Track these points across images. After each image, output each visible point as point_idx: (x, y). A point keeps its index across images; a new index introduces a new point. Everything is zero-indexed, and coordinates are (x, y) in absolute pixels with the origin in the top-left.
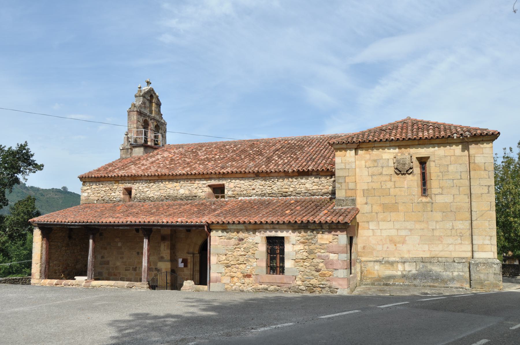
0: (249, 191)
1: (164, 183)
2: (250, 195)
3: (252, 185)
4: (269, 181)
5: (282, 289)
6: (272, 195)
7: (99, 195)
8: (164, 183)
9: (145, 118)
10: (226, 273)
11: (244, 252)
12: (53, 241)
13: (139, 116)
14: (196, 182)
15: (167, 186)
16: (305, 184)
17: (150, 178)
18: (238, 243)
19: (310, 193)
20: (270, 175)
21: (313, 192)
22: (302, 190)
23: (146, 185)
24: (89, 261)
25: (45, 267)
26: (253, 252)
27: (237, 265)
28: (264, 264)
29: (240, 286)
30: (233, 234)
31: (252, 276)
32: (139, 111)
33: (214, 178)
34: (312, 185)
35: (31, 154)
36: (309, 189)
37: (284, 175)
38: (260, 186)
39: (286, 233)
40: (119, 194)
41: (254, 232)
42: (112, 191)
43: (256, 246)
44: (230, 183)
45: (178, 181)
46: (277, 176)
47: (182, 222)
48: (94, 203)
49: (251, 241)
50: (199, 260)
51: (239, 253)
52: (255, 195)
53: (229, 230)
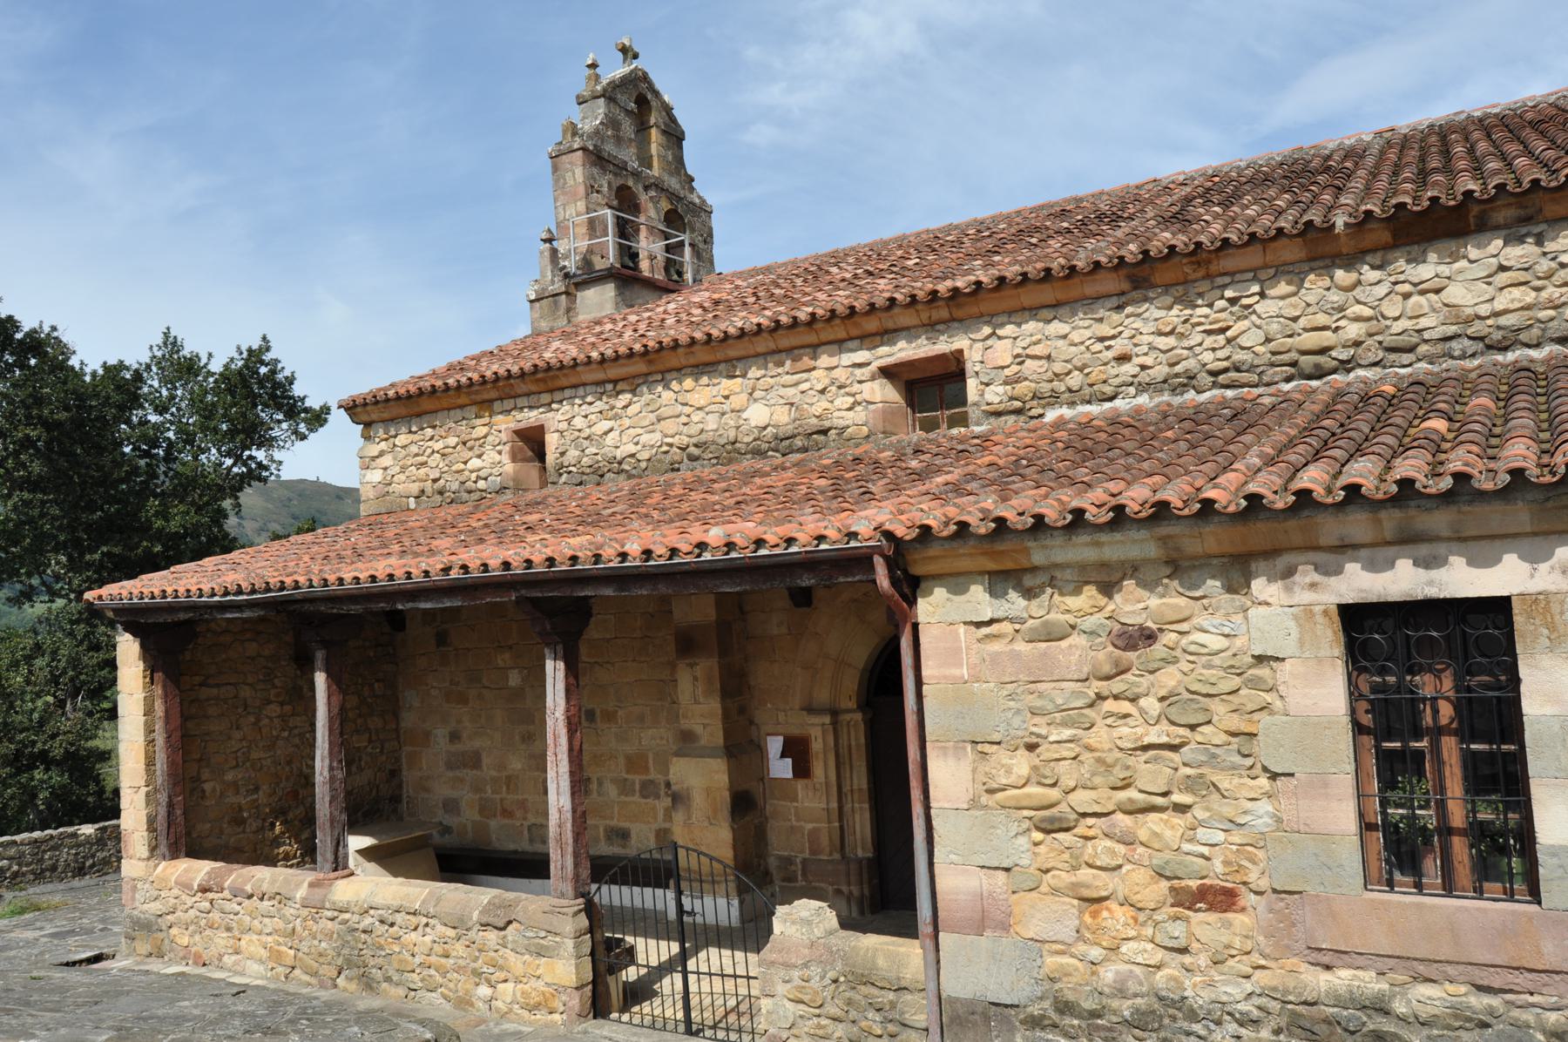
0: (1096, 373)
1: (675, 385)
2: (1108, 390)
3: (1113, 337)
4: (1210, 305)
5: (1528, 1016)
6: (1233, 375)
7: (423, 471)
8: (675, 385)
9: (620, 182)
10: (1047, 871)
11: (1164, 726)
12: (210, 681)
13: (595, 171)
14: (819, 363)
15: (689, 398)
16: (1438, 291)
17: (613, 372)
18: (1117, 663)
19: (1482, 339)
20: (1213, 268)
21: (1499, 328)
22: (1424, 322)
23: (599, 405)
24: (318, 779)
25: (170, 805)
26: (1236, 723)
27: (1119, 816)
28: (1344, 818)
29: (1158, 967)
30: (1073, 602)
31: (1242, 902)
32: (591, 148)
33: (907, 329)
34: (1490, 289)
35: (286, 378)
36: (1469, 311)
37: (1303, 255)
38: (1161, 334)
39: (1525, 567)
40: (498, 458)
41: (1236, 576)
42: (471, 449)
43: (1260, 679)
44: (989, 342)
45: (735, 367)
46: (1255, 270)
47: (730, 546)
48: (408, 509)
49: (1216, 643)
50: (863, 741)
51: (1125, 730)
52: (1132, 390)
53: (1042, 578)
